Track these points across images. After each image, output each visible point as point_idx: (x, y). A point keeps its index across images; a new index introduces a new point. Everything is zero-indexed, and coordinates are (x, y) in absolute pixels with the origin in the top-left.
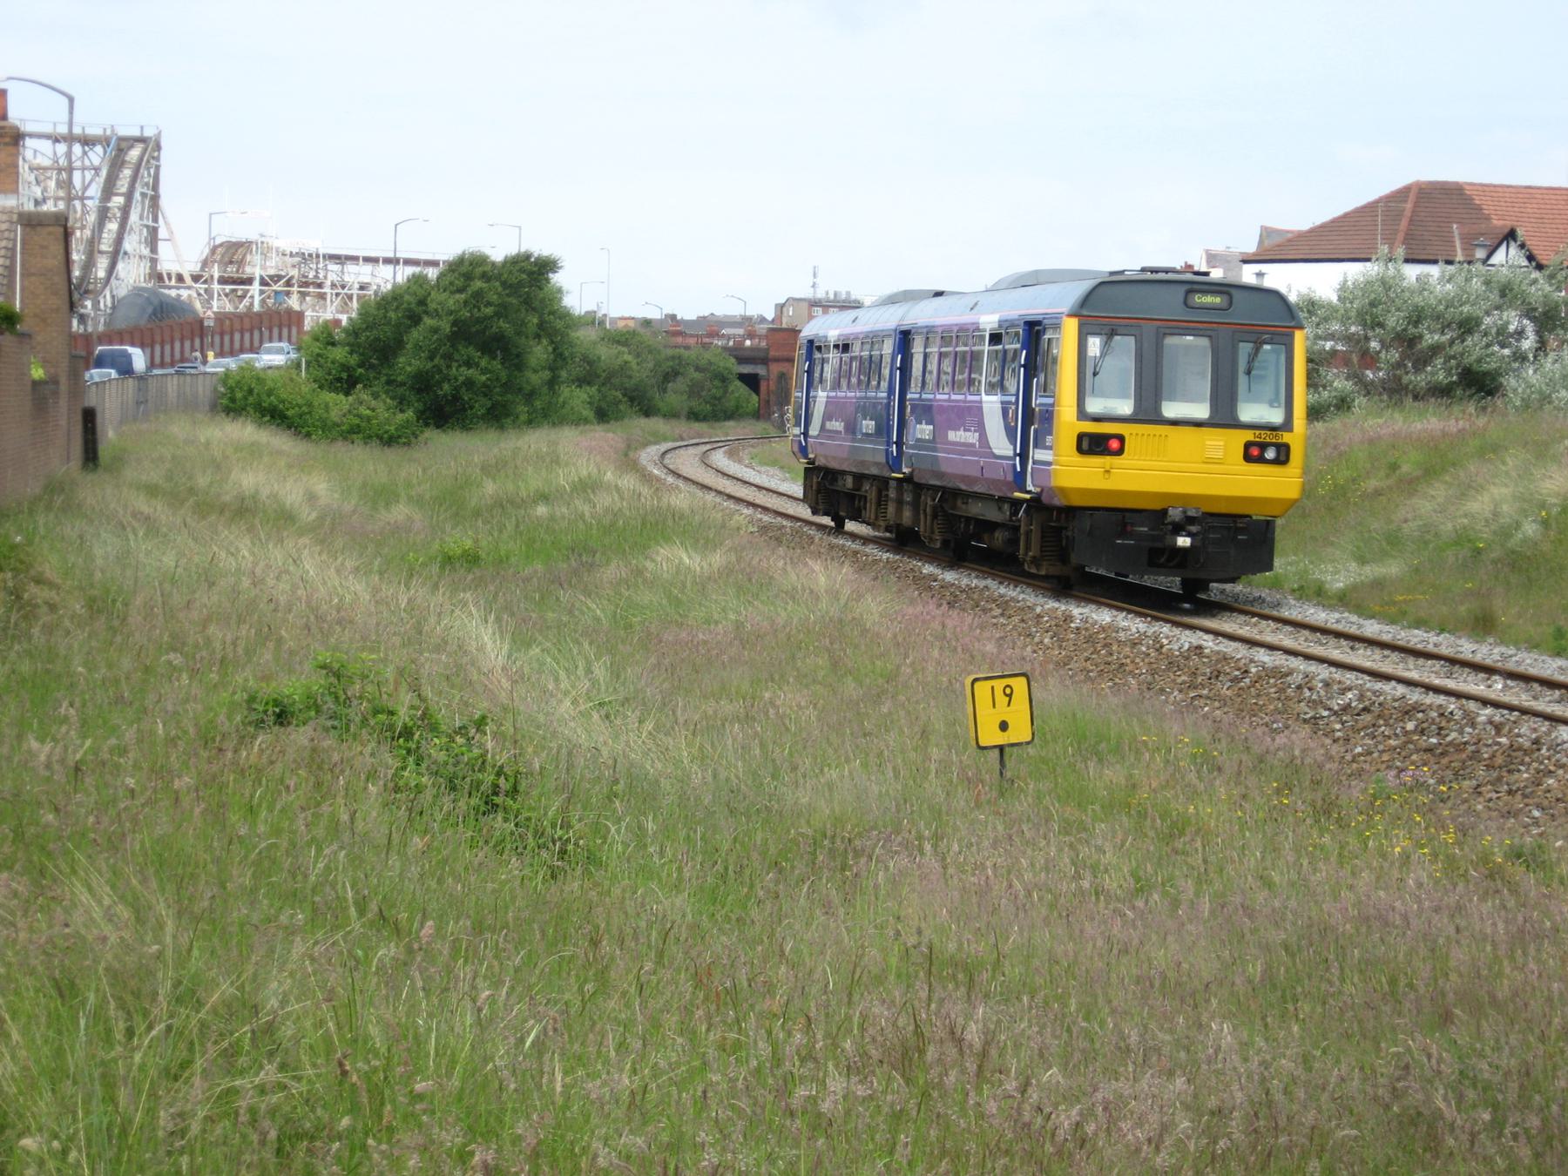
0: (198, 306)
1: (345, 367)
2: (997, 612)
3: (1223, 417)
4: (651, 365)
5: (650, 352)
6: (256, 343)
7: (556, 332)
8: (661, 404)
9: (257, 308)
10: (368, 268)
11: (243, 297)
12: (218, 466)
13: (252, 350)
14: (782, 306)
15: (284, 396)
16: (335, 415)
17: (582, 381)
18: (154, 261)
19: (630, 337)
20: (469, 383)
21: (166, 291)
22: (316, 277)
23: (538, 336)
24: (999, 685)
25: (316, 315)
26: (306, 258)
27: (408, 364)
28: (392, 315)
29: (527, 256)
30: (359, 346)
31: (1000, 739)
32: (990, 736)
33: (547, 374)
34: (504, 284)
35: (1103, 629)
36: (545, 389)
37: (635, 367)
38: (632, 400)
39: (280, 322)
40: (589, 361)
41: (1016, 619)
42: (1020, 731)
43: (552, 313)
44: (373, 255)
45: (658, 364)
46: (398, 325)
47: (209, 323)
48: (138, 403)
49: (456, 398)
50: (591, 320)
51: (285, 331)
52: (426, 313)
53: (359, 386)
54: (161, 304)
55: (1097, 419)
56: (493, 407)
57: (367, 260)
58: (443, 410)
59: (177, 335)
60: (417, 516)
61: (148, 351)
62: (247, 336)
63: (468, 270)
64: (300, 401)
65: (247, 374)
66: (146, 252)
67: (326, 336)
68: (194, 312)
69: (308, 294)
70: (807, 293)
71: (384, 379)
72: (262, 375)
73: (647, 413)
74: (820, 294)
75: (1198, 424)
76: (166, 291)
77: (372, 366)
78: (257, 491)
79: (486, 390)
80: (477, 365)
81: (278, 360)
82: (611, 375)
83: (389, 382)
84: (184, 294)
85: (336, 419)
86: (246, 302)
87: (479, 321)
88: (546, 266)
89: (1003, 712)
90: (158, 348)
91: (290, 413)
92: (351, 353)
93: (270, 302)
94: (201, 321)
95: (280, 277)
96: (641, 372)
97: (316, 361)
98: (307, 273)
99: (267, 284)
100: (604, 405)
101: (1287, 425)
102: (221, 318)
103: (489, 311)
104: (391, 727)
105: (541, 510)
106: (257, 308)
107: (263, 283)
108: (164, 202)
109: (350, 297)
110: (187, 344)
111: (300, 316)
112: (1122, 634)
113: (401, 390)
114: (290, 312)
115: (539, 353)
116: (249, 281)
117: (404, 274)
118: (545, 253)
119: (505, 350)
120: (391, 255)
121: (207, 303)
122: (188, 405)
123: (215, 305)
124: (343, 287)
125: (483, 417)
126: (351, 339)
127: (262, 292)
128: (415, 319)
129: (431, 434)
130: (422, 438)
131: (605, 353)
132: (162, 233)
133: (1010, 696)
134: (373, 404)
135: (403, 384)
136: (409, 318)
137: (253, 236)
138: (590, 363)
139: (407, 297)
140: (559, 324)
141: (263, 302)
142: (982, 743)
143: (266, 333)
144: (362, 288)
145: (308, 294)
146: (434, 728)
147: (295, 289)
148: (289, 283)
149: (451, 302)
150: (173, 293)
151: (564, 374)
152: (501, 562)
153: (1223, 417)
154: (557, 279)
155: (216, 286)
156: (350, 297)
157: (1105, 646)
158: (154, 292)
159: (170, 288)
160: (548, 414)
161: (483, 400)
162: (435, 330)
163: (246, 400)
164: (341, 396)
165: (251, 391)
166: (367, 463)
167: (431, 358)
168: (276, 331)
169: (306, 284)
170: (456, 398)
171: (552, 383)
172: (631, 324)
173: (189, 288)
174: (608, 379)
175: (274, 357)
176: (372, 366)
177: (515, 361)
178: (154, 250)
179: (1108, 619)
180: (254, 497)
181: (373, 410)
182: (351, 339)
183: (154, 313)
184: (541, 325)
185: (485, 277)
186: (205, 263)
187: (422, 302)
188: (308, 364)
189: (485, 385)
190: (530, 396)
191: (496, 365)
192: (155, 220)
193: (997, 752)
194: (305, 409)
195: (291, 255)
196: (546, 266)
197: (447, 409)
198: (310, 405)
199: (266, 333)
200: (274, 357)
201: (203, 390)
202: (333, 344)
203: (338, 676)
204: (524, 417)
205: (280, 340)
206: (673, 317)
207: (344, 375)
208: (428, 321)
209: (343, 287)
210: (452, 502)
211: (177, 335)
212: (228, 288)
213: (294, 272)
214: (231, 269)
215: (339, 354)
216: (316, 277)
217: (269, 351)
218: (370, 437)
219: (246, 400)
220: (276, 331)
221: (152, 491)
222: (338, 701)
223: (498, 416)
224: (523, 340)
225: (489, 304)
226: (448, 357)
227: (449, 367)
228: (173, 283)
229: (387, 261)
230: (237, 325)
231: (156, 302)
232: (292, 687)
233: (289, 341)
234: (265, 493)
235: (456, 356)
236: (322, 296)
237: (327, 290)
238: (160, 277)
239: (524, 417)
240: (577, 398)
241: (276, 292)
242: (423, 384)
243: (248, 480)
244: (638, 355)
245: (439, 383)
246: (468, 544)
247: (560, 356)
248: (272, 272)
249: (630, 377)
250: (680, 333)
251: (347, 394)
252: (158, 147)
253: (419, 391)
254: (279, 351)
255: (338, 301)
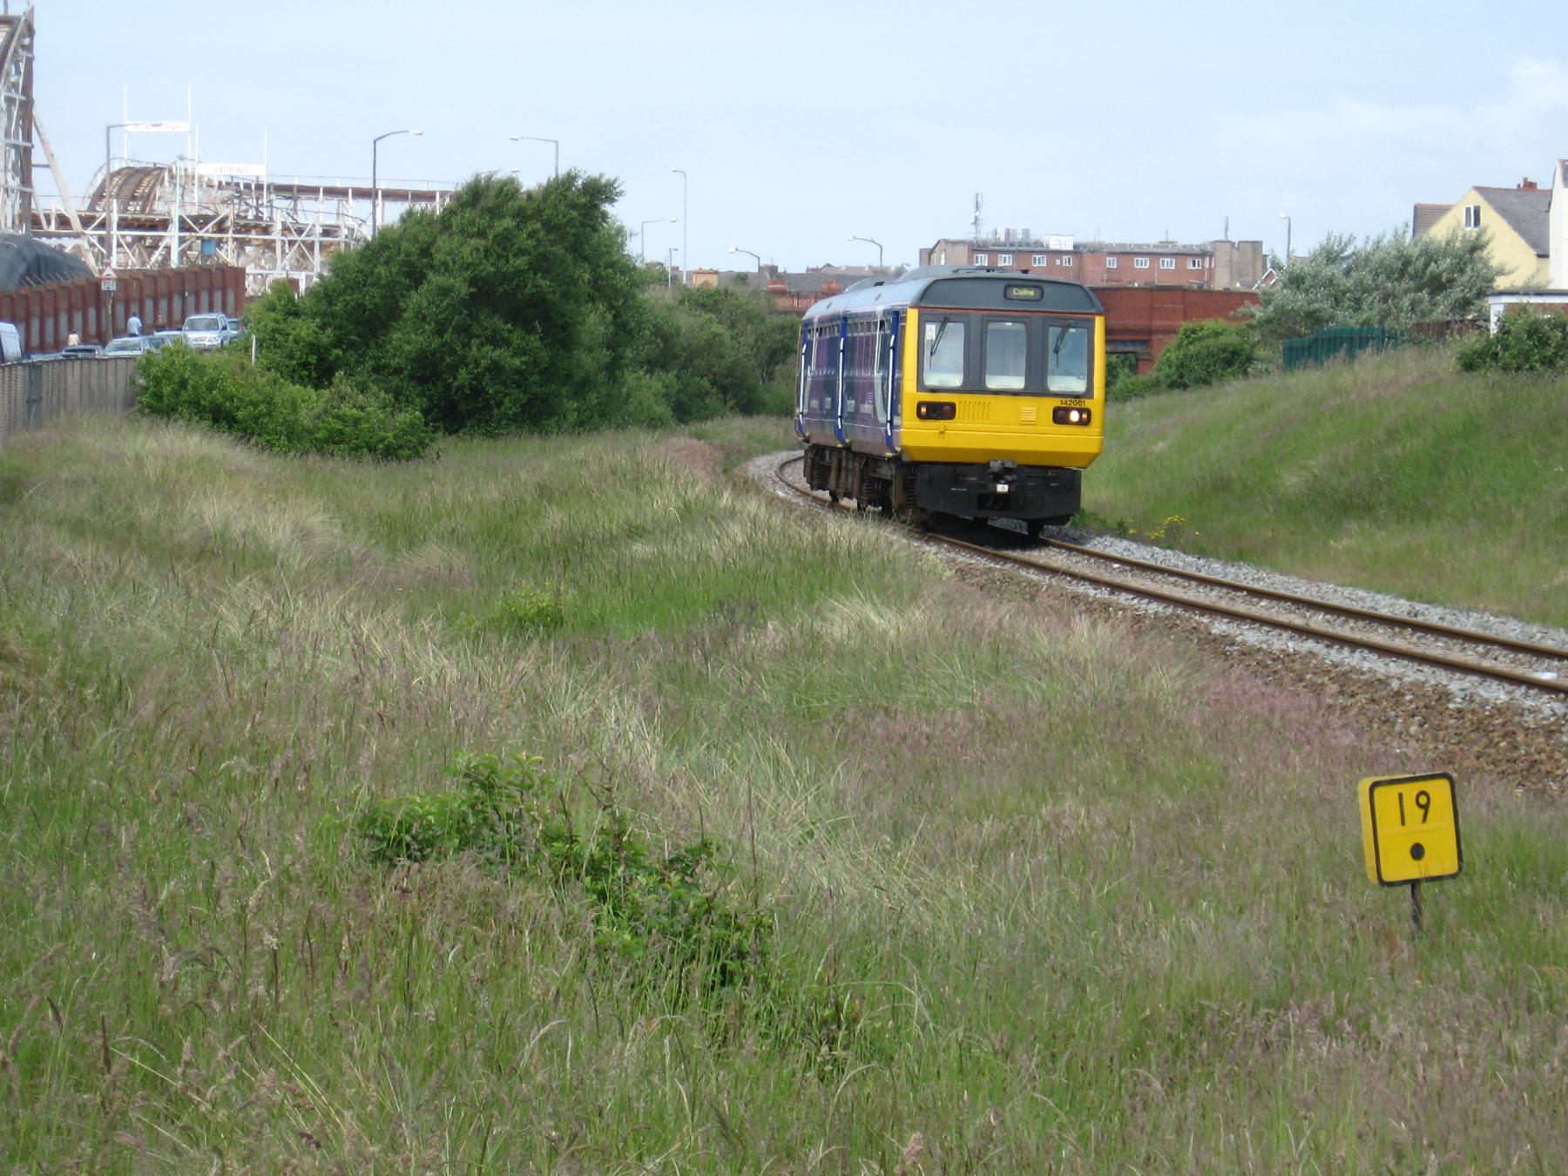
0: (91, 261)
1: (314, 348)
2: (1334, 688)
3: (1036, 388)
4: (751, 340)
5: (749, 320)
6: (177, 315)
7: (617, 291)
8: (767, 397)
9: (174, 262)
10: (332, 204)
11: (155, 247)
12: (167, 490)
13: (171, 324)
14: (931, 251)
15: (231, 389)
16: (305, 418)
17: (655, 364)
18: (26, 197)
19: (719, 298)
20: (496, 368)
21: (44, 240)
22: (258, 218)
23: (592, 299)
24: (1410, 790)
25: (262, 275)
26: (242, 190)
27: (405, 341)
28: (382, 270)
29: (570, 179)
30: (333, 316)
31: (1413, 870)
32: (1399, 867)
33: (605, 355)
34: (549, 227)
35: (1499, 711)
36: (602, 377)
37: (727, 340)
38: (724, 390)
39: (214, 285)
40: (665, 336)
41: (1362, 698)
42: (1441, 859)
43: (612, 265)
44: (339, 184)
45: (761, 338)
46: (392, 285)
47: (109, 286)
48: (29, 402)
49: (477, 391)
50: (660, 276)
51: (218, 296)
52: (432, 267)
53: (340, 374)
54: (38, 259)
55: (933, 390)
56: (533, 399)
57: (331, 192)
58: (457, 405)
59: (63, 304)
60: (459, 560)
61: (23, 327)
62: (163, 304)
63: (485, 200)
64: (255, 397)
65: (178, 360)
66: (15, 183)
67: (284, 300)
68: (84, 268)
69: (249, 242)
70: (965, 232)
71: (370, 364)
72: (202, 360)
73: (749, 407)
74: (985, 234)
75: (1015, 393)
76: (44, 240)
77: (352, 345)
78: (226, 527)
79: (520, 379)
80: (508, 343)
81: (209, 338)
82: (693, 354)
83: (377, 369)
84: (69, 244)
85: (307, 422)
86: (157, 255)
87: (506, 278)
88: (599, 192)
89: (1416, 831)
90: (35, 324)
91: (240, 414)
92: (323, 327)
93: (193, 253)
94: (97, 285)
95: (207, 219)
96: (738, 349)
97: (270, 341)
98: (245, 212)
99: (190, 229)
100: (684, 398)
101: (1089, 393)
102: (126, 279)
103: (521, 262)
104: (571, 860)
105: (640, 549)
106: (174, 262)
107: (184, 226)
108: (39, 111)
109: (311, 247)
110: (63, 319)
111: (239, 274)
112: (1529, 720)
113: (395, 381)
114: (224, 269)
115: (594, 322)
116: (164, 225)
117: (392, 214)
118: (594, 172)
119: (546, 319)
120: (368, 185)
121: (102, 259)
122: (95, 401)
123: (113, 259)
124: (300, 231)
125: (514, 419)
126: (324, 307)
127: (182, 240)
128: (416, 277)
129: (443, 443)
130: (431, 451)
131: (686, 322)
132: (37, 156)
133: (1426, 807)
134: (357, 400)
135: (398, 371)
136: (408, 275)
137: (163, 161)
138: (666, 338)
139: (405, 245)
140: (620, 281)
141: (183, 253)
142: (1387, 877)
143: (191, 301)
144: (326, 233)
145: (249, 242)
146: (633, 862)
147: (230, 235)
148: (221, 228)
149: (466, 251)
150: (53, 242)
151: (629, 353)
152: (595, 625)
153: (1036, 388)
154: (618, 212)
155: (115, 232)
156: (311, 247)
157: (1504, 736)
158: (27, 242)
159: (50, 235)
160: (604, 413)
161: (515, 393)
162: (445, 292)
163: (172, 395)
164: (311, 390)
165: (183, 384)
166: (374, 486)
167: (440, 332)
168: (204, 297)
169: (247, 228)
170: (477, 391)
171: (613, 368)
172: (714, 281)
173: (77, 236)
174: (690, 359)
175: (204, 334)
176: (352, 345)
177: (561, 335)
178: (26, 180)
179: (1503, 697)
180: (223, 534)
181: (362, 409)
182: (324, 307)
183: (28, 272)
184: (595, 283)
185: (521, 216)
186: (99, 196)
187: (426, 252)
188: (260, 344)
189: (518, 372)
190: (582, 387)
191: (534, 341)
192: (28, 137)
193: (1408, 889)
194: (263, 408)
195: (220, 186)
196: (599, 192)
197: (462, 406)
198: (269, 401)
199: (191, 301)
200: (204, 334)
201: (117, 384)
202: (296, 314)
203: (488, 787)
204: (572, 417)
205: (211, 310)
206: (773, 269)
207: (313, 359)
208: (435, 279)
209: (300, 231)
210: (500, 538)
211: (63, 304)
212: (131, 234)
213: (224, 211)
214: (134, 208)
215: (305, 329)
216: (258, 218)
217: (193, 328)
218: (357, 448)
219: (172, 395)
220: (204, 297)
221: (78, 528)
222: (483, 819)
223: (536, 415)
224: (571, 306)
225: (521, 252)
226: (465, 331)
227: (466, 345)
228: (53, 228)
229: (361, 194)
230: (148, 290)
231: (30, 255)
232: (418, 800)
233: (224, 310)
234: (236, 529)
235: (476, 329)
236: (269, 246)
237: (276, 235)
238: (35, 222)
239: (572, 417)
240: (647, 387)
241: (203, 240)
242: (427, 370)
243: (214, 510)
244: (733, 326)
245: (454, 369)
246: (546, 599)
247: (622, 331)
248: (194, 212)
249: (722, 356)
250: (783, 293)
251: (317, 387)
252: (30, 31)
253: (422, 380)
254: (212, 326)
255: (292, 253)
